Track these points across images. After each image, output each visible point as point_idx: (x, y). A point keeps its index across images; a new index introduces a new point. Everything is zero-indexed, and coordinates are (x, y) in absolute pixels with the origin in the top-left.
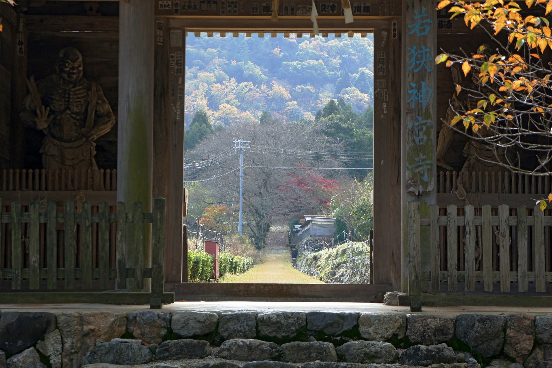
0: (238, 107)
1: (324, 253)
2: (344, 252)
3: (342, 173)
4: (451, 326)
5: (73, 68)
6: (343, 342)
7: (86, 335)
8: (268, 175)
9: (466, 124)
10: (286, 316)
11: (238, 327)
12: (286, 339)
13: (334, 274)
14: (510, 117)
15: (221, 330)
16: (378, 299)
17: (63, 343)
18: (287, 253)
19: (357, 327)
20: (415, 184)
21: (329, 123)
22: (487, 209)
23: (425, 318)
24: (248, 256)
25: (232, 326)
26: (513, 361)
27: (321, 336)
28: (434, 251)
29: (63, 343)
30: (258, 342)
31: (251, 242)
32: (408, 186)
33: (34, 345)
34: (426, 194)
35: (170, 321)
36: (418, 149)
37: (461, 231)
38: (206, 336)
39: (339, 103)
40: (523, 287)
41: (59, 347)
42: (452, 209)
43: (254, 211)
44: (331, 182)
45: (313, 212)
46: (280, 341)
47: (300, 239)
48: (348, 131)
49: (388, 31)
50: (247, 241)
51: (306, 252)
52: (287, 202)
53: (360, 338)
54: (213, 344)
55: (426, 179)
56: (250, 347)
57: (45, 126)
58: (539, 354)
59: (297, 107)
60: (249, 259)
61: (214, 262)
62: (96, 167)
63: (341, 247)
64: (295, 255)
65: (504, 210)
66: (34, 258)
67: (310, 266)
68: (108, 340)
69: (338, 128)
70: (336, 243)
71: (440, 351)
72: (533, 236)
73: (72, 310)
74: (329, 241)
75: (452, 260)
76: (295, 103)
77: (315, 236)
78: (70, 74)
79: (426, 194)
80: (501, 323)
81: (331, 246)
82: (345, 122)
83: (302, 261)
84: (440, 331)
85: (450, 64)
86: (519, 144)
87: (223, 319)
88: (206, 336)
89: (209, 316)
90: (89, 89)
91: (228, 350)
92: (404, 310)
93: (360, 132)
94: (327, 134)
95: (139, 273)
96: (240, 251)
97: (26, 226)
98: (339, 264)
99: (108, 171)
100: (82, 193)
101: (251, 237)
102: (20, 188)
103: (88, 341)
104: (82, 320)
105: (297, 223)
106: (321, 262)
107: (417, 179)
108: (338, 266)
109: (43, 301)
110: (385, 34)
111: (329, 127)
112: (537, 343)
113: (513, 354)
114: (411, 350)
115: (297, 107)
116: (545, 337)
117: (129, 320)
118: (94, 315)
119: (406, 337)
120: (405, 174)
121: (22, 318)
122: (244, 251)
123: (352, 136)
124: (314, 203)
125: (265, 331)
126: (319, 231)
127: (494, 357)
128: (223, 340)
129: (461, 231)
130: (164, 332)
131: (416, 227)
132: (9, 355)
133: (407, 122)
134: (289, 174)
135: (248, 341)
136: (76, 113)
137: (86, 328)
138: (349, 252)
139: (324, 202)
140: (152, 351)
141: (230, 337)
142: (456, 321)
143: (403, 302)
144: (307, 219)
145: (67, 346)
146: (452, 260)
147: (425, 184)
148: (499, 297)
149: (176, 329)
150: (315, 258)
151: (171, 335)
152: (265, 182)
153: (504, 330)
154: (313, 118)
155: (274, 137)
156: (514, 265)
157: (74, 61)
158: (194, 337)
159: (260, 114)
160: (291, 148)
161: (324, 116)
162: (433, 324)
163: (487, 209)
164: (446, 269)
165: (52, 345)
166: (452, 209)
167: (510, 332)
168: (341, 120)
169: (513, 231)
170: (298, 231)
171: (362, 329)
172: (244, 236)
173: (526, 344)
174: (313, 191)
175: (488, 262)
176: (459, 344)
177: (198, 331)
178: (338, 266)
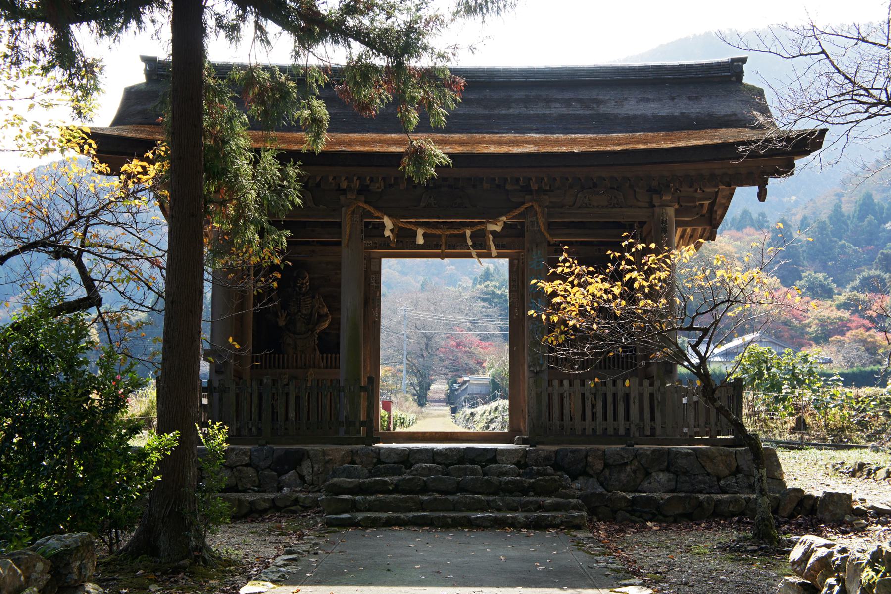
0: (400, 272)
1: (480, 409)
2: (496, 409)
3: (497, 336)
4: (553, 455)
5: (303, 284)
6: (486, 465)
7: (327, 462)
8: (429, 338)
9: (550, 340)
10: (451, 450)
11: (421, 457)
12: (452, 464)
13: (488, 427)
14: (573, 337)
15: (411, 459)
16: (511, 442)
17: (313, 467)
18: (447, 410)
19: (495, 457)
20: (534, 365)
21: (485, 289)
23: (537, 451)
24: (412, 412)
25: (417, 456)
26: (591, 476)
27: (473, 462)
28: (545, 408)
29: (313, 467)
30: (434, 465)
31: (414, 400)
32: (529, 367)
33: (295, 468)
34: (541, 371)
35: (379, 453)
38: (402, 463)
39: (495, 270)
40: (599, 431)
41: (311, 470)
42: (556, 383)
43: (413, 370)
44: (487, 344)
45: (472, 371)
46: (448, 466)
47: (458, 396)
49: (519, 260)
50: (411, 399)
51: (464, 409)
52: (447, 363)
53: (496, 462)
54: (407, 468)
55: (541, 362)
56: (429, 468)
57: (284, 323)
58: (607, 472)
59: (455, 272)
60: (413, 416)
61: (389, 418)
62: (318, 353)
63: (493, 405)
64: (454, 411)
66: (292, 415)
67: (468, 420)
68: (341, 465)
70: (490, 400)
71: (545, 470)
73: (318, 447)
74: (483, 399)
76: (454, 267)
77: (472, 394)
78: (301, 288)
79: (541, 371)
80: (584, 453)
81: (485, 403)
82: (500, 288)
83: (459, 415)
84: (547, 459)
85: (535, 315)
87: (411, 451)
88: (402, 463)
89: (403, 451)
90: (314, 298)
91: (416, 470)
92: (526, 447)
94: (484, 300)
95: (358, 424)
96: (405, 409)
97: (287, 394)
98: (492, 419)
99: (334, 356)
100: (311, 371)
101: (414, 395)
102: (270, 367)
103: (328, 466)
104: (324, 453)
105: (456, 382)
106: (477, 418)
108: (491, 421)
109: (298, 443)
110: (516, 262)
111: (486, 293)
112: (606, 466)
113: (591, 472)
114: (528, 470)
115: (455, 272)
116: (611, 461)
117: (353, 453)
118: (332, 450)
119: (526, 463)
121: (287, 452)
122: (408, 408)
124: (472, 363)
125: (438, 459)
126: (476, 390)
127: (580, 475)
128: (412, 465)
130: (375, 461)
132: (279, 475)
134: (448, 338)
135: (428, 465)
136: (306, 315)
137: (327, 458)
138: (500, 409)
139: (480, 364)
140: (370, 471)
141: (417, 463)
142: (557, 452)
143: (524, 441)
144: (465, 379)
145: (315, 469)
147: (541, 366)
148: (585, 438)
149: (382, 458)
150: (472, 414)
151: (380, 462)
152: (427, 345)
153: (586, 457)
154: (470, 283)
155: (434, 304)
156: (615, 418)
157: (303, 279)
158: (395, 463)
159: (421, 279)
160: (450, 314)
161: (480, 283)
162: (543, 454)
164: (562, 420)
165: (306, 468)
167: (590, 459)
168: (495, 287)
170: (457, 390)
171: (498, 458)
172: (407, 395)
173: (599, 466)
174: (470, 353)
176: (557, 467)
177: (396, 460)
178: (491, 421)
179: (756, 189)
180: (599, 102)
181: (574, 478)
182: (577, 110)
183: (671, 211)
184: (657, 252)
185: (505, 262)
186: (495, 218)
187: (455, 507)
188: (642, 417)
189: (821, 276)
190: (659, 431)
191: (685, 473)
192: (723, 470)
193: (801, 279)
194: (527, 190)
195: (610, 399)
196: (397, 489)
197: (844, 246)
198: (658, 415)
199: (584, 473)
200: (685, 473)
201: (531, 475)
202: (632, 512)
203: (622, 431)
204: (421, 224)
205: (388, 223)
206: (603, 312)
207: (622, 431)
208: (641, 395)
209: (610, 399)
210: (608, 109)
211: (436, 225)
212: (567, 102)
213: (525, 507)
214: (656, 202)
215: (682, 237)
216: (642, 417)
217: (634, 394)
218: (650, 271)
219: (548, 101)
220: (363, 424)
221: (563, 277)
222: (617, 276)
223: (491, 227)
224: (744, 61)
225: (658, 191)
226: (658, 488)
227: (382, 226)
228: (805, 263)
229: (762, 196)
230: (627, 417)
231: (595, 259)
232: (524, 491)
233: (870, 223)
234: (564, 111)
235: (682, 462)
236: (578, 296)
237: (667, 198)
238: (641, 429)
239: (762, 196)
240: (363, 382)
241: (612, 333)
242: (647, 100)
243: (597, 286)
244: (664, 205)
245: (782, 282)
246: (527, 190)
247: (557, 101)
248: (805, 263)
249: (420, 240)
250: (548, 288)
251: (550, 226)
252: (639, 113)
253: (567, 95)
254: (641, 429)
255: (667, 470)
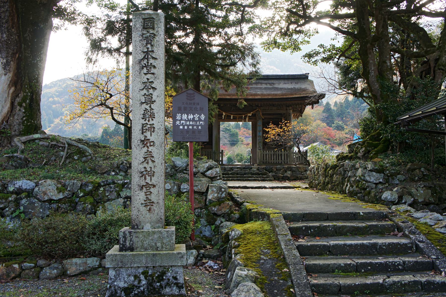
22: (270, 151)
36: (259, 142)
37: (266, 155)
48: (229, 130)
65: (272, 151)
69: (226, 129)
72: (296, 81)
75: (265, 159)
84: (263, 169)
86: (235, 42)
93: (233, 130)
107: (259, 147)
111: (224, 129)
112: (277, 170)
120: (258, 146)
123: (231, 132)
129: (266, 155)
131: (260, 154)
133: (258, 138)
146: (265, 159)
163: (270, 151)
166: (265, 151)
169: (274, 154)
173: (275, 170)
175: (270, 159)
179: (311, 106)
180: (274, 84)
181: (270, 173)
182: (269, 86)
183: (291, 111)
184: (289, 123)
185: (251, 123)
186: (250, 112)
187: (245, 177)
188: (285, 159)
189: (340, 123)
190: (288, 162)
191: (294, 171)
192: (303, 170)
193: (334, 123)
194: (258, 106)
195: (277, 155)
196: (231, 174)
197: (349, 112)
198: (288, 159)
199: (272, 172)
200: (294, 171)
201: (260, 171)
202: (283, 179)
203: (280, 162)
204: (232, 114)
205: (224, 114)
206: (279, 135)
207: (280, 162)
208: (284, 154)
209: (277, 155)
210: (276, 86)
211: (236, 114)
212: (266, 84)
213: (260, 177)
214: (288, 109)
215: (294, 116)
216: (285, 159)
217: (283, 154)
218: (288, 127)
219: (261, 83)
220: (221, 161)
221: (270, 128)
222: (281, 128)
223: (249, 115)
224: (309, 74)
225: (288, 106)
226: (289, 174)
227: (223, 114)
228: (336, 118)
229: (312, 108)
230: (281, 159)
231: (277, 124)
232: (259, 174)
233: (358, 104)
234: (266, 86)
235: (294, 169)
236: (274, 132)
237: (290, 108)
238: (285, 162)
239: (312, 108)
240: (221, 152)
241: (280, 139)
242: (285, 83)
243: (278, 130)
244: (290, 110)
245: (327, 125)
246: (258, 106)
247: (263, 83)
248: (336, 118)
249: (232, 118)
250: (267, 130)
251: (263, 114)
252: (283, 87)
253: (266, 82)
254: (285, 162)
255: (290, 171)
